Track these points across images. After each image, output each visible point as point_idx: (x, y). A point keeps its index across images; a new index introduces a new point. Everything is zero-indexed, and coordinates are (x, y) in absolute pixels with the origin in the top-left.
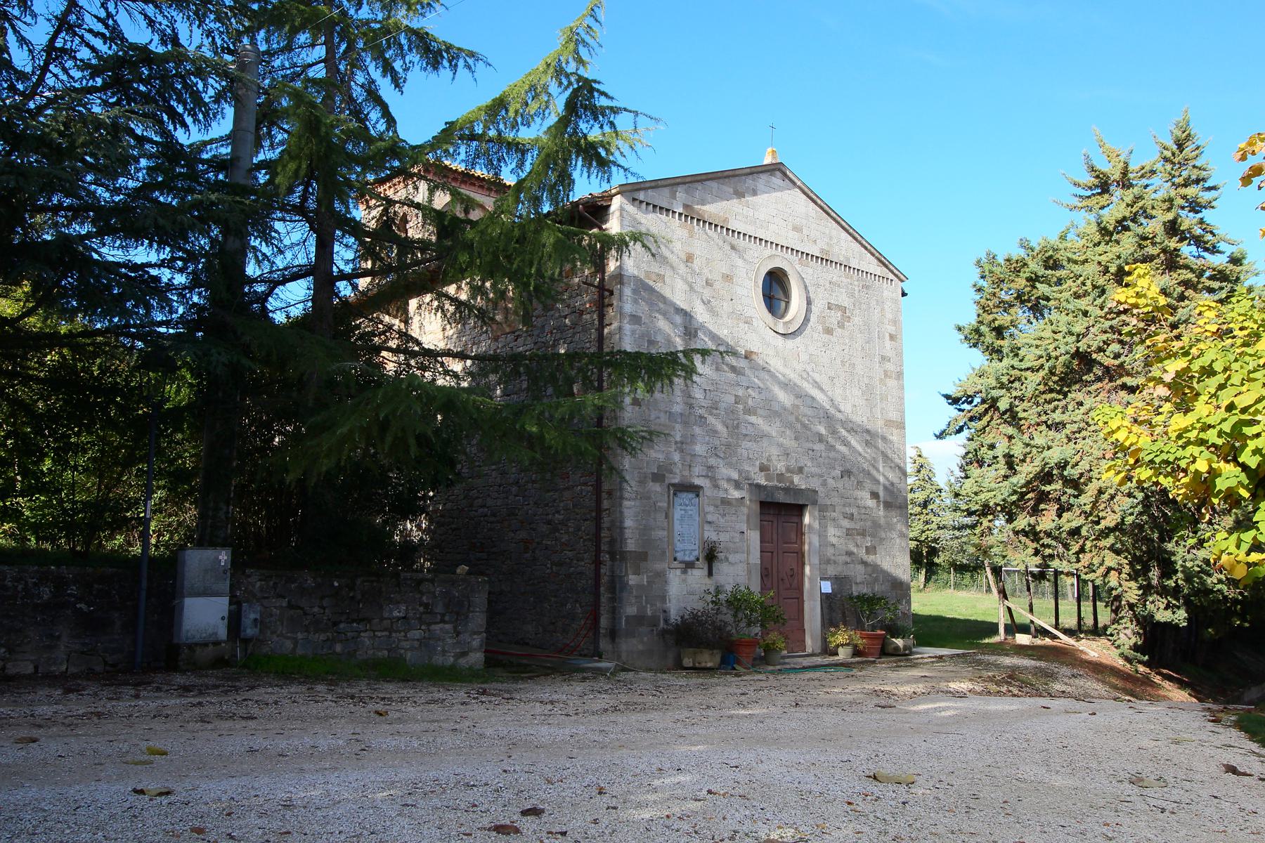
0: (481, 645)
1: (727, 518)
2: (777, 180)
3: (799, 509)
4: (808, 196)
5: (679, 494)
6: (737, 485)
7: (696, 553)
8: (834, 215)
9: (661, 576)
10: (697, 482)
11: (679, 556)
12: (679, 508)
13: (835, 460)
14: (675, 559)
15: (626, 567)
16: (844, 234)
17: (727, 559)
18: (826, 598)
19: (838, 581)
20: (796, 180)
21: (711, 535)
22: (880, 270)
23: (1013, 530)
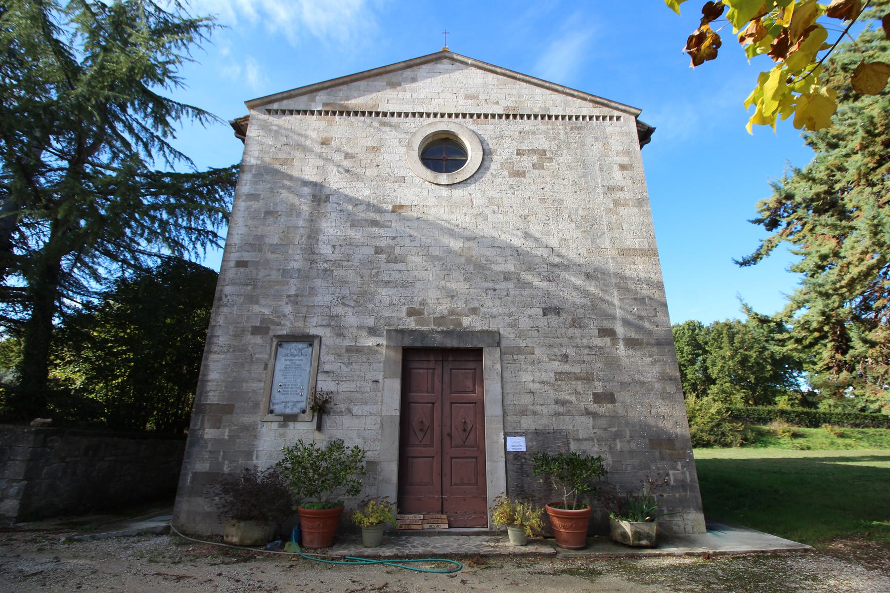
0: (18, 493)
1: (354, 366)
2: (445, 65)
3: (477, 353)
4: (485, 69)
5: (285, 345)
6: (373, 331)
7: (303, 405)
8: (521, 77)
9: (251, 431)
10: (313, 331)
11: (278, 408)
12: (283, 359)
13: (533, 297)
14: (271, 412)
15: (203, 422)
16: (539, 90)
17: (349, 411)
18: (513, 458)
19: (536, 435)
20: (465, 60)
21: (326, 385)
22: (597, 111)
23: (518, 150)
